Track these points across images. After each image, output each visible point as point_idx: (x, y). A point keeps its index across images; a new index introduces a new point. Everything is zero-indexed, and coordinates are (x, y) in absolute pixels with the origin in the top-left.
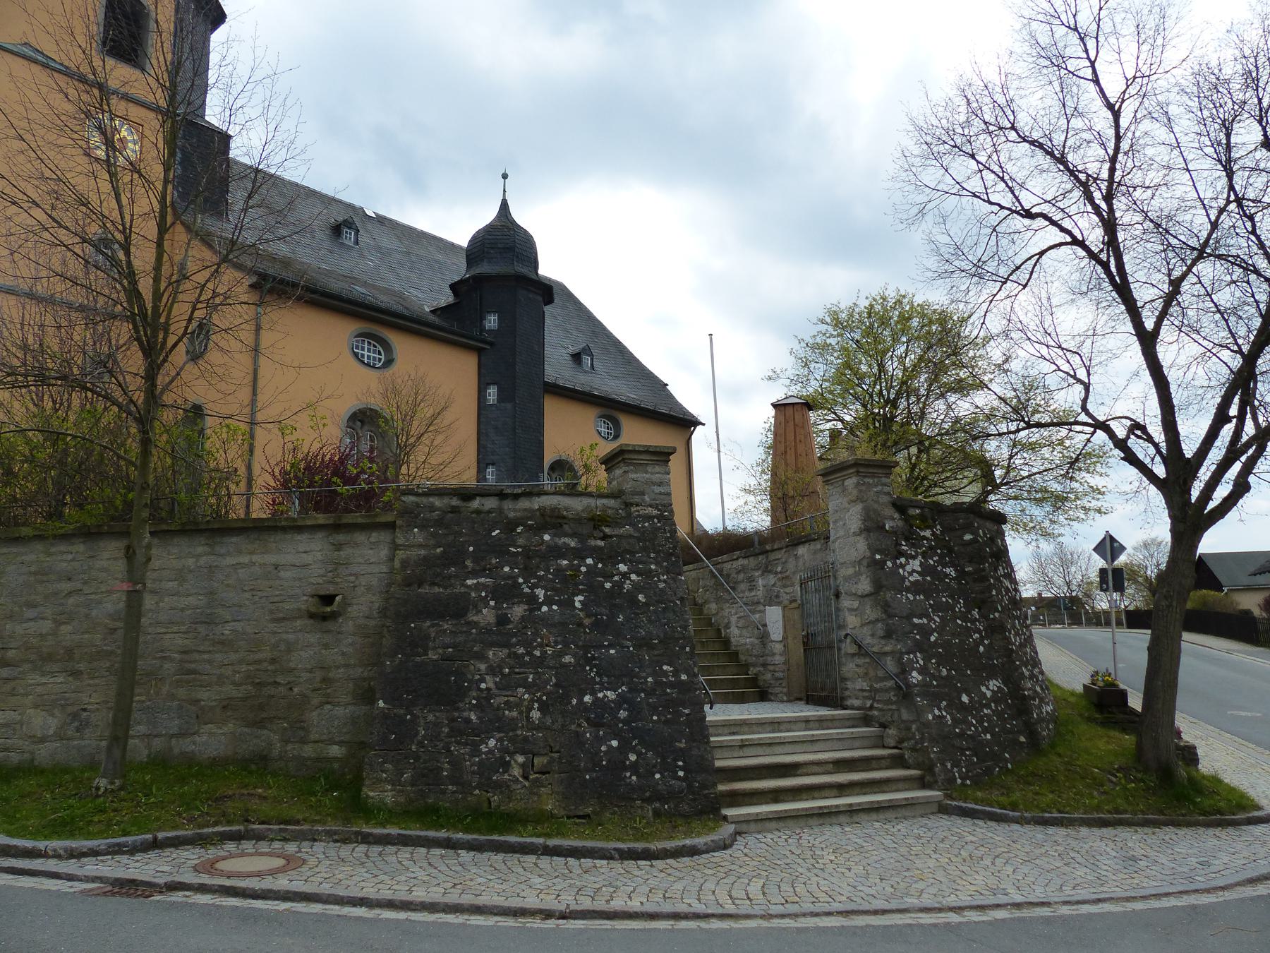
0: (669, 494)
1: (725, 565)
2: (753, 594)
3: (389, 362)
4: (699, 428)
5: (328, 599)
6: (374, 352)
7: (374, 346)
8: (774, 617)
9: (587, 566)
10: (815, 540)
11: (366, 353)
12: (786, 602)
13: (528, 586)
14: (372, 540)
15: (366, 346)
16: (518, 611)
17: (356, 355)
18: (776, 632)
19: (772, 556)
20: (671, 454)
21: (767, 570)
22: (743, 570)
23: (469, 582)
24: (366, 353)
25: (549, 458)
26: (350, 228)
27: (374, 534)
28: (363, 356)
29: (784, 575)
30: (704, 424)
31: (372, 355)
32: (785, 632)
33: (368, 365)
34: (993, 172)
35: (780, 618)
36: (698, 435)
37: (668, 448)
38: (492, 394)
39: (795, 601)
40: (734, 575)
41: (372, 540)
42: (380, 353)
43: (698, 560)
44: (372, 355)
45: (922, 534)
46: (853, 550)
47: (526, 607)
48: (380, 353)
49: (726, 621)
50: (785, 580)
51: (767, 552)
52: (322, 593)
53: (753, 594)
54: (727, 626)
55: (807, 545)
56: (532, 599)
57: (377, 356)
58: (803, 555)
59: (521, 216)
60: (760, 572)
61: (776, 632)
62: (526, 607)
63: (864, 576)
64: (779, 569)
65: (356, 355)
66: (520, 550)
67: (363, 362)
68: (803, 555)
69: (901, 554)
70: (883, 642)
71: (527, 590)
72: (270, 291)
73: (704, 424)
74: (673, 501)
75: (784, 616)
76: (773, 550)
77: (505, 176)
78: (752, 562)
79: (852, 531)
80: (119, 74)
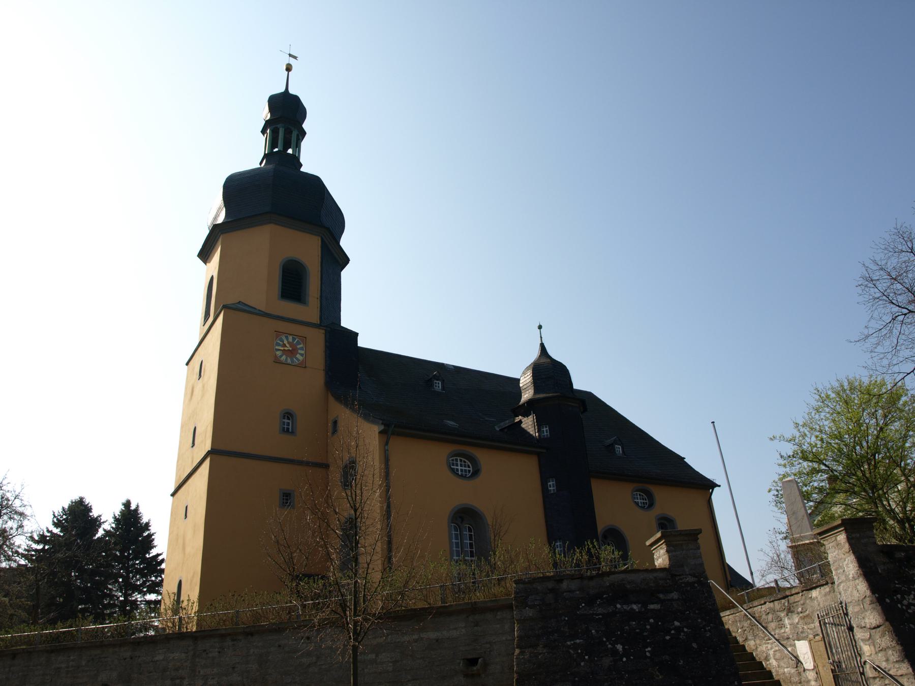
0: (702, 564)
1: (755, 609)
2: (783, 631)
3: (476, 473)
4: (716, 489)
5: (473, 662)
6: (465, 467)
7: (465, 462)
8: (803, 649)
9: (650, 624)
10: (823, 585)
11: (459, 468)
12: (811, 636)
13: (610, 644)
14: (498, 617)
15: (459, 463)
16: (607, 661)
17: (453, 470)
18: (808, 662)
19: (792, 599)
20: (699, 534)
21: (790, 611)
22: (773, 611)
23: (569, 643)
24: (459, 468)
25: (601, 527)
26: (437, 380)
27: (499, 613)
28: (457, 470)
29: (805, 614)
30: (719, 486)
31: (463, 468)
32: (815, 661)
33: (462, 476)
34: (899, 316)
35: (808, 650)
36: (719, 498)
37: (696, 530)
38: (552, 485)
39: (818, 635)
40: (764, 617)
41: (498, 617)
42: (469, 467)
43: (734, 606)
44: (463, 468)
45: (789, 669)
46: (855, 592)
47: (611, 659)
48: (469, 467)
49: (765, 655)
50: (806, 618)
51: (787, 596)
52: (470, 657)
53: (783, 631)
54: (767, 659)
55: (818, 589)
56: (615, 652)
57: (467, 469)
58: (817, 598)
59: (555, 354)
60: (785, 612)
61: (808, 662)
62: (611, 659)
63: (869, 612)
64: (800, 609)
65: (453, 470)
66: (600, 616)
67: (458, 474)
68: (817, 598)
69: (896, 591)
70: (897, 665)
71: (610, 646)
72: (393, 434)
73: (719, 486)
74: (706, 568)
75: (811, 648)
76: (792, 595)
77: (540, 327)
78: (777, 605)
79: (851, 576)
80: (290, 309)
